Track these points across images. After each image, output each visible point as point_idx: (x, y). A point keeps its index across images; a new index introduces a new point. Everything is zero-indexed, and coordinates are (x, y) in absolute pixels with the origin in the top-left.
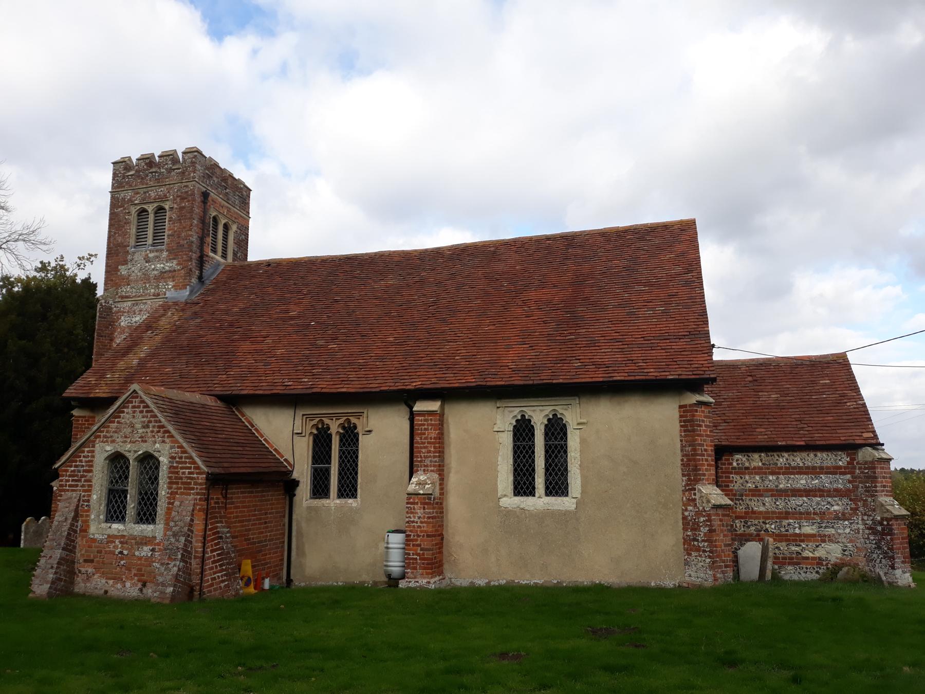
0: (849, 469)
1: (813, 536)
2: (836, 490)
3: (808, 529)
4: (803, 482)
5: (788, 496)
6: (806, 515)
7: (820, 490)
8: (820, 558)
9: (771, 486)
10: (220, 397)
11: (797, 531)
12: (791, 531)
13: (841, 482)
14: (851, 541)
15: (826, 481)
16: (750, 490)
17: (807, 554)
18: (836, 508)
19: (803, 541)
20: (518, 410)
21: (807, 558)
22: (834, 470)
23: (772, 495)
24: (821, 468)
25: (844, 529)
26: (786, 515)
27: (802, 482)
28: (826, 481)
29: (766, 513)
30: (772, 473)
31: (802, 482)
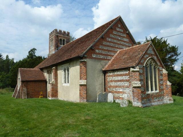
0: (129, 74)
1: (122, 92)
2: (126, 80)
3: (121, 90)
4: (120, 78)
5: (117, 82)
6: (120, 87)
7: (123, 80)
8: (123, 98)
9: (114, 79)
10: (40, 69)
11: (119, 91)
12: (117, 91)
13: (127, 78)
14: (129, 93)
15: (124, 78)
16: (111, 81)
17: (121, 96)
18: (126, 85)
19: (120, 93)
20: (67, 66)
21: (121, 98)
22: (126, 75)
23: (114, 82)
24: (123, 74)
25: (127, 90)
26: (117, 87)
27: (120, 78)
28: (124, 78)
29: (113, 86)
30: (114, 76)
31: (120, 78)
